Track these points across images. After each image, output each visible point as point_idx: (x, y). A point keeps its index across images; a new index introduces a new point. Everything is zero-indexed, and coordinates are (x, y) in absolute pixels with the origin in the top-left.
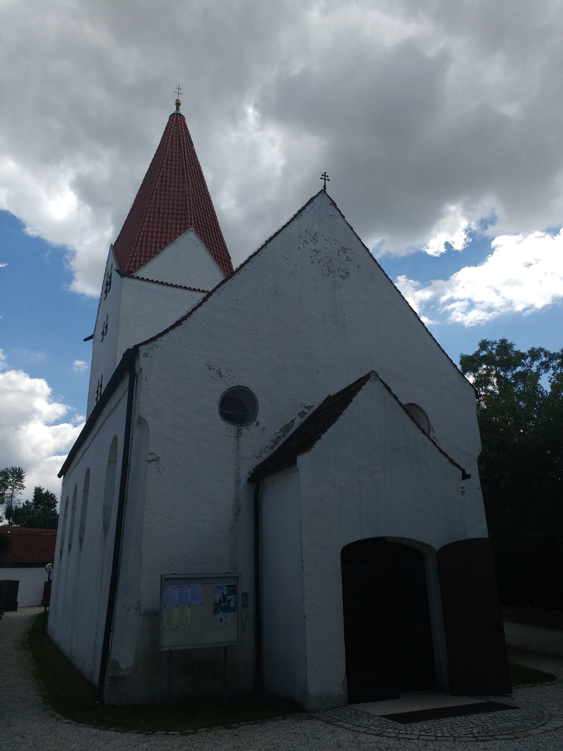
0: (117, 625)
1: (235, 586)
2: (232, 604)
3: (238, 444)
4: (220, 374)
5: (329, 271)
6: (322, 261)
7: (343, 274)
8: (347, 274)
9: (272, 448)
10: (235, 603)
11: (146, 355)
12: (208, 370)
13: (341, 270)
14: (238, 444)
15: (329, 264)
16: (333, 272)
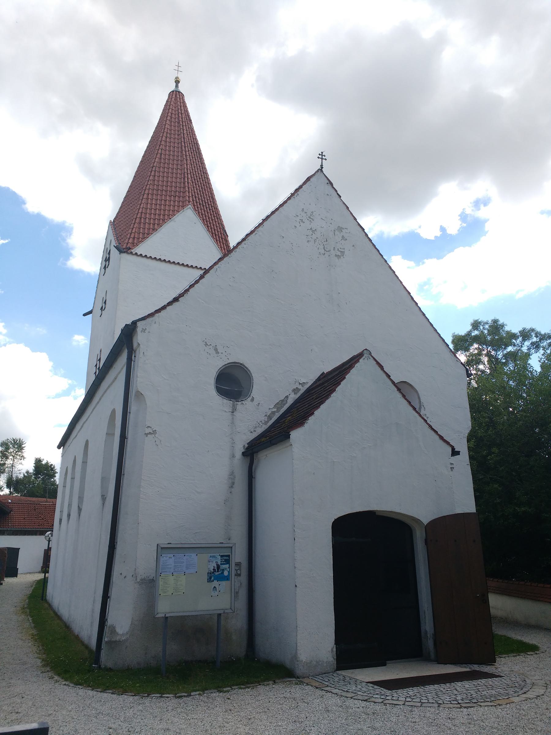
0: (114, 592)
1: (229, 556)
2: (226, 573)
3: (233, 419)
4: (216, 350)
5: (325, 250)
6: (318, 240)
7: (339, 253)
8: (343, 253)
9: (266, 423)
10: (229, 572)
11: (144, 330)
12: (204, 346)
13: (336, 249)
14: (233, 419)
15: (325, 243)
16: (329, 251)
